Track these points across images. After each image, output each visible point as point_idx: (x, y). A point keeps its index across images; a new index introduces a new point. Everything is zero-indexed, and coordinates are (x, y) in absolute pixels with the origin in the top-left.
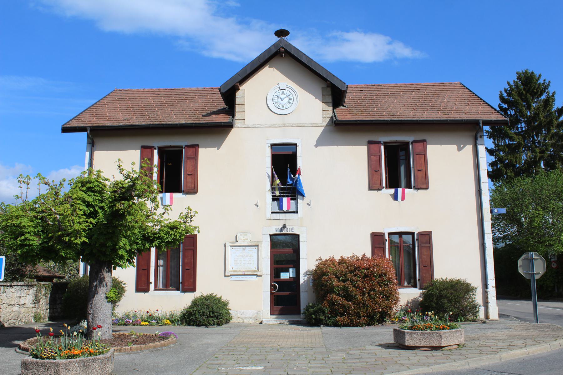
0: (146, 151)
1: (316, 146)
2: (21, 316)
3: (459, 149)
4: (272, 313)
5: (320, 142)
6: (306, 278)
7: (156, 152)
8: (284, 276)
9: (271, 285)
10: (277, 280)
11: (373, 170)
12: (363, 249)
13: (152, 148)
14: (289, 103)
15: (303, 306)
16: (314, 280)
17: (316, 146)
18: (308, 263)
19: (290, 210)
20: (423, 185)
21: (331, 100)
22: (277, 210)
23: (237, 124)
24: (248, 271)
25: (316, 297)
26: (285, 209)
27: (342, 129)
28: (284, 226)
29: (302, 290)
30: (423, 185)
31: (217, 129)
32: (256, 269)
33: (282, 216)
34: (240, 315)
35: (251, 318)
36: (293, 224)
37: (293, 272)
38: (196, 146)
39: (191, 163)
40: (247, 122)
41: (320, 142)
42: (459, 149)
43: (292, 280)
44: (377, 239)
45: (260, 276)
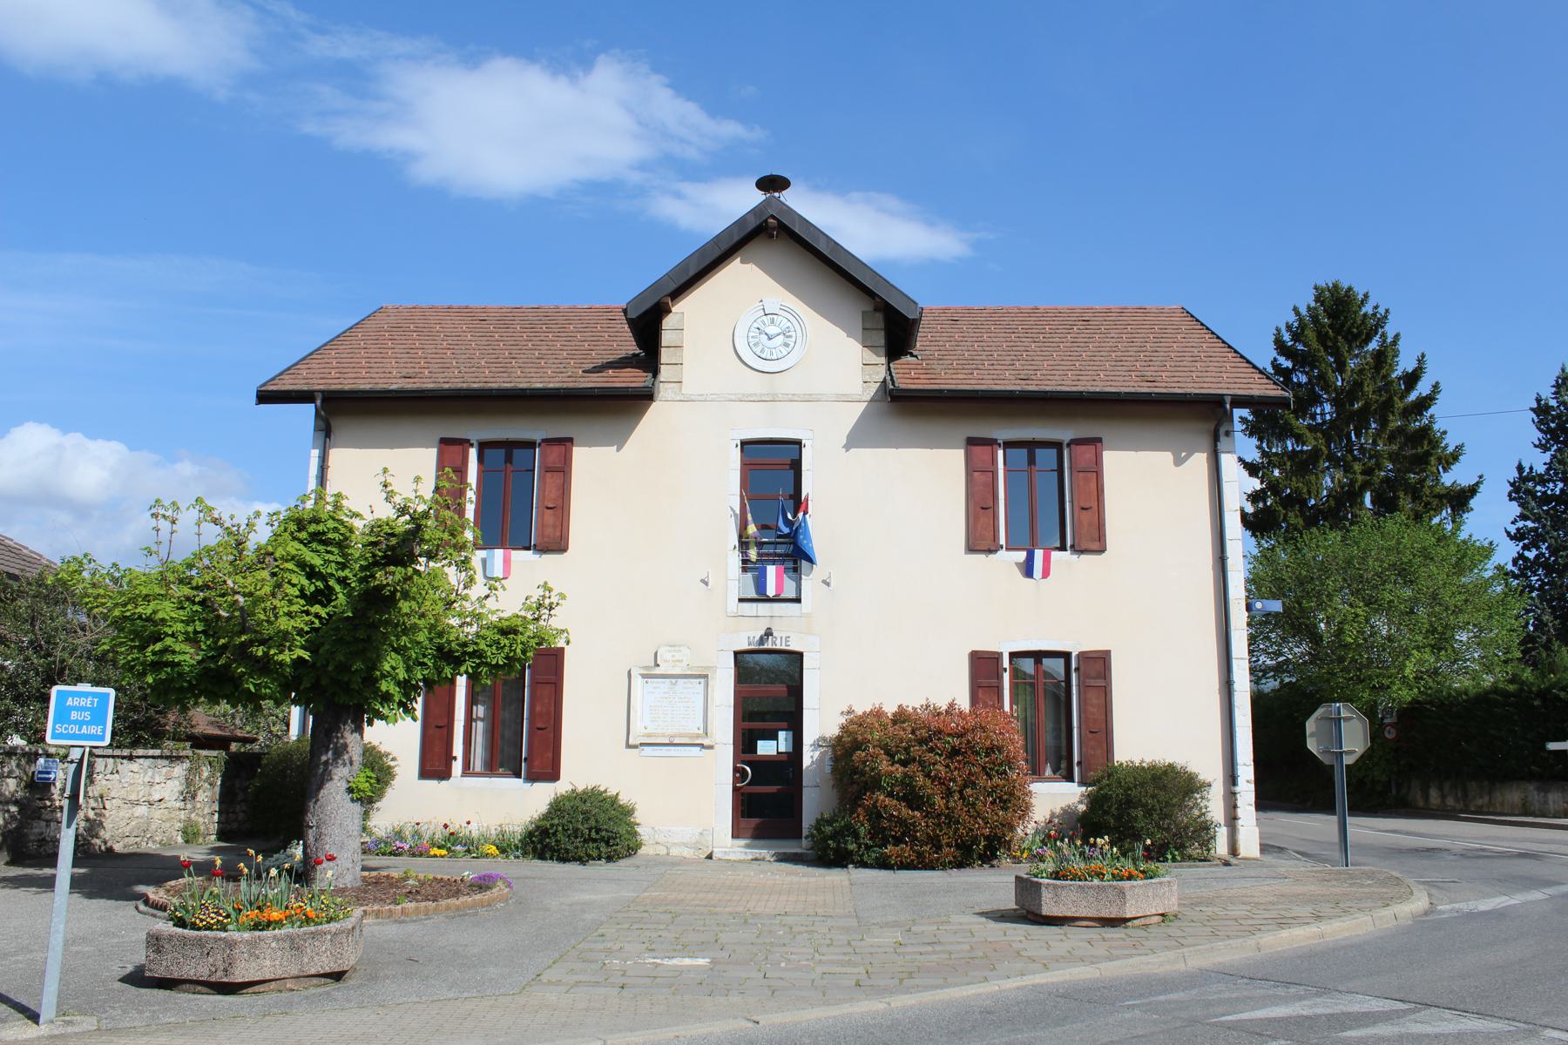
0: (451, 448)
1: (847, 447)
2: (153, 827)
3: (1178, 462)
4: (736, 834)
5: (856, 439)
6: (817, 754)
7: (473, 453)
8: (765, 748)
9: (736, 770)
10: (749, 757)
11: (979, 507)
12: (949, 689)
13: (465, 443)
14: (786, 345)
15: (808, 818)
16: (836, 759)
17: (847, 447)
18: (822, 720)
19: (783, 596)
20: (1092, 540)
21: (882, 342)
22: (754, 595)
23: (664, 391)
24: (681, 736)
25: (849, 801)
26: (771, 592)
27: (907, 408)
28: (769, 633)
30: (1092, 540)
31: (618, 403)
33: (763, 608)
34: (660, 838)
36: (790, 629)
38: (567, 442)
39: (553, 480)
40: (687, 389)
41: (856, 439)
42: (1178, 462)
43: (785, 758)
44: (984, 666)
45: (711, 747)
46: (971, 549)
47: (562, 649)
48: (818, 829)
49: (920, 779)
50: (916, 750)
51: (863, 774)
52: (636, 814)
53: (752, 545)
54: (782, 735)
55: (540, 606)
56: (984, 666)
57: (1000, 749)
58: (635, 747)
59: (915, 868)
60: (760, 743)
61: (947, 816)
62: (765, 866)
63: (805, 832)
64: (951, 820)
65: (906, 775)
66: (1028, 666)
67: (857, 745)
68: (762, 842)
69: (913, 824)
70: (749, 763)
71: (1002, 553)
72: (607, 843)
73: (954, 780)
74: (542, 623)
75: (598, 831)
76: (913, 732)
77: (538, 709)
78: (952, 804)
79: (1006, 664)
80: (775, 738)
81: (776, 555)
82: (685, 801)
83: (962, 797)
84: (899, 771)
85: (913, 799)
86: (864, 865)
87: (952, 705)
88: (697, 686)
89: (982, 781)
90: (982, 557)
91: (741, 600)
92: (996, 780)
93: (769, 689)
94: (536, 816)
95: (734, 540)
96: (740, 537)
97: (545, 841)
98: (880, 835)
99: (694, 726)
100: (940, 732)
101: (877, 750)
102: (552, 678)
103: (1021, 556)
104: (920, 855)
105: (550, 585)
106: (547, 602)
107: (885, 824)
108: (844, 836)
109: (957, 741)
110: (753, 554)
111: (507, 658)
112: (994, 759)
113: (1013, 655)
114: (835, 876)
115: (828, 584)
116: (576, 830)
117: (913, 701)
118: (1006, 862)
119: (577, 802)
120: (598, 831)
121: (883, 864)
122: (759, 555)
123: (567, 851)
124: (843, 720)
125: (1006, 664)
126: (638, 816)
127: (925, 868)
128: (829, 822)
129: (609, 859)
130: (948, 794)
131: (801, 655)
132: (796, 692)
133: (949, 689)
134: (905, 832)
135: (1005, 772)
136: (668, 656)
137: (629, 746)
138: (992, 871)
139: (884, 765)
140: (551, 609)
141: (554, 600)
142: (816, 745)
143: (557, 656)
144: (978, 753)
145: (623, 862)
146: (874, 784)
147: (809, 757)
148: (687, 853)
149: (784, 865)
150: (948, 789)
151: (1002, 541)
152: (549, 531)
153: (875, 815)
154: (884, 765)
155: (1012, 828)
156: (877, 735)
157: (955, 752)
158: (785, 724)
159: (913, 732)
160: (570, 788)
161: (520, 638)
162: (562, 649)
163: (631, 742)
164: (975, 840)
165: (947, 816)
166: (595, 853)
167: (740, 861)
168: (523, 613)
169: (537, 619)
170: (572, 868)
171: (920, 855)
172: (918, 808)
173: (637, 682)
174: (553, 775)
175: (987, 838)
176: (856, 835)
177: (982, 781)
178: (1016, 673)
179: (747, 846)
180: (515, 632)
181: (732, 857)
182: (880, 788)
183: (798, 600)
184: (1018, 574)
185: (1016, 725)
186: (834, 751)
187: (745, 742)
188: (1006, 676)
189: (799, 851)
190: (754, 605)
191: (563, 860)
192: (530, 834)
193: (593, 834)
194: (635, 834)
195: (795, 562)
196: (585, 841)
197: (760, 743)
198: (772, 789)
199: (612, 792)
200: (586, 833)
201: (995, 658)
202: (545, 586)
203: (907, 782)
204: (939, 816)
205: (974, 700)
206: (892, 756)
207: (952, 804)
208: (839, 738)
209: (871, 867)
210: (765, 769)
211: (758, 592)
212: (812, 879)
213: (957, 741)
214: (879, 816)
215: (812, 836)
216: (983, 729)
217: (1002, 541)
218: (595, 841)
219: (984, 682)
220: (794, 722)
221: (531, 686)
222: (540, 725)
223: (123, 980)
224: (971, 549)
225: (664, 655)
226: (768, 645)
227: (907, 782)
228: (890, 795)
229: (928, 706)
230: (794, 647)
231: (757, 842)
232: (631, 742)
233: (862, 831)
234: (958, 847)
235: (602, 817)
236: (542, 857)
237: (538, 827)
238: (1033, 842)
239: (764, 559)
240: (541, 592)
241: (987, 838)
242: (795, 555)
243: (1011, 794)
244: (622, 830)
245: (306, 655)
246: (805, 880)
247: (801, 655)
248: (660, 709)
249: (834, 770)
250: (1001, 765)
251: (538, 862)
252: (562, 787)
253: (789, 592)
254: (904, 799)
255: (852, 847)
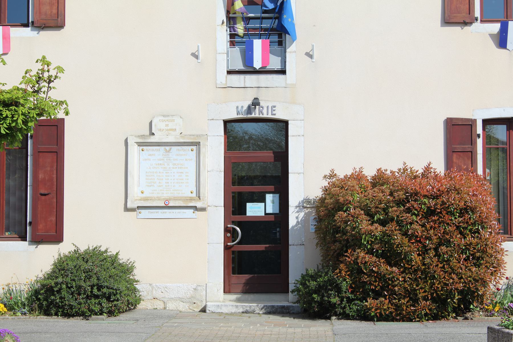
4: (227, 291)
6: (302, 215)
8: (254, 210)
9: (226, 230)
10: (239, 218)
15: (294, 275)
16: (320, 220)
18: (305, 185)
19: (269, 67)
22: (240, 66)
24: (175, 199)
26: (257, 64)
28: (256, 103)
29: (292, 240)
32: (194, 195)
33: (251, 80)
34: (158, 294)
35: (182, 300)
36: (276, 98)
37: (273, 202)
43: (272, 218)
44: (458, 133)
45: (203, 209)
46: (448, 21)
47: (63, 120)
48: (303, 284)
49: (398, 238)
50: (394, 211)
51: (344, 233)
52: (135, 272)
53: (239, 20)
54: (269, 197)
55: (39, 79)
56: (458, 133)
57: (473, 210)
58: (133, 210)
59: (393, 320)
60: (249, 205)
61: (423, 272)
62: (254, 318)
63: (291, 287)
64: (427, 275)
65: (384, 234)
66: (500, 132)
67: (339, 207)
68: (252, 296)
69: (391, 279)
70: (239, 224)
71: (477, 26)
72: (108, 299)
73: (429, 238)
74: (42, 95)
75: (100, 288)
76: (391, 194)
77: (41, 176)
78: (427, 261)
79: (479, 130)
80: (262, 199)
81: (261, 29)
82: (181, 260)
83: (438, 255)
84: (378, 230)
85: (391, 255)
86: (346, 317)
87: (428, 169)
88: (189, 153)
89: (456, 239)
90: (457, 29)
91: (229, 72)
92: (469, 239)
93: (257, 156)
94: (41, 275)
95: (222, 16)
96: (228, 12)
97: (49, 299)
98: (361, 291)
99: (187, 189)
100: (416, 194)
101: (358, 211)
102: (54, 147)
103: (496, 27)
104: (398, 307)
105: (48, 59)
106: (46, 75)
107: (365, 278)
108: (327, 290)
109: (432, 203)
110: (240, 28)
111: (9, 128)
112: (468, 217)
113: (486, 122)
114: (319, 327)
115: (311, 57)
116: (79, 287)
117: (392, 165)
118: (479, 315)
119: (80, 262)
120: (100, 288)
121: (364, 316)
122: (246, 29)
123: (71, 307)
124: (325, 183)
125: (479, 130)
126: (138, 274)
127: (403, 319)
128: (313, 278)
129: (111, 313)
130: (425, 251)
131: (286, 123)
132: (282, 157)
133: (425, 154)
134: (384, 287)
135: (478, 231)
136: (162, 126)
137: (127, 209)
138: (466, 322)
139: (364, 225)
140: (50, 82)
141: (53, 73)
142: (301, 206)
143: (57, 128)
144: (452, 214)
145: (122, 316)
146: (355, 242)
147: (294, 218)
148: (183, 307)
149: (272, 317)
150: (424, 246)
151: (477, 13)
152: (46, 8)
153: (356, 271)
154: (364, 225)
155: (484, 283)
156: (357, 197)
157: (431, 212)
158: (272, 188)
159: (391, 194)
160: (73, 249)
161: (21, 109)
162: (63, 120)
163: (129, 205)
164: (450, 294)
165: (423, 272)
166: (97, 309)
167: (232, 314)
168: (23, 86)
169: (37, 92)
170: (76, 322)
171: (398, 307)
172: (396, 265)
173: (134, 149)
174: (57, 237)
175: (461, 292)
176: (338, 290)
177: (456, 239)
178: (488, 139)
179: (238, 300)
180: (17, 104)
181: (225, 310)
182: (360, 245)
183: (283, 72)
184: (491, 45)
185: (490, 187)
186: (318, 212)
187: (235, 204)
188: (480, 142)
189: (286, 304)
190: (242, 77)
191: (67, 315)
192: (36, 292)
193: (95, 291)
194: (135, 290)
195: (280, 36)
196: (88, 297)
197: (249, 205)
198: (261, 247)
199: (112, 251)
200: (90, 288)
201: (470, 124)
202: (44, 60)
203: (386, 240)
204: (416, 271)
205: (449, 164)
206: (372, 216)
207: (427, 261)
208: (322, 200)
209: (353, 318)
210: (253, 230)
211: (245, 65)
212: (299, 330)
213: (432, 203)
214: (360, 271)
215: (298, 290)
216: (458, 191)
217: (477, 13)
218: (96, 297)
219: (459, 147)
220: (281, 185)
221: (33, 155)
222: (42, 192)
223: (200, 311)
224: (448, 21)
225: (158, 125)
226: (256, 114)
227: (386, 240)
228: (370, 252)
229: (405, 170)
230: (280, 115)
231: (247, 296)
232: (129, 205)
233: (344, 286)
234: (434, 300)
235: (103, 275)
236: (47, 313)
237: (43, 286)
238: (505, 296)
239: (251, 34)
240: (39, 66)
241: (461, 292)
242: (278, 32)
243: (484, 252)
244: (122, 286)
245: (460, 297)
246: (291, 330)
247: (286, 123)
248: (158, 175)
249: (318, 230)
250: (474, 224)
251: (44, 318)
252: (65, 248)
253: (275, 63)
254: (383, 255)
255: (335, 300)
